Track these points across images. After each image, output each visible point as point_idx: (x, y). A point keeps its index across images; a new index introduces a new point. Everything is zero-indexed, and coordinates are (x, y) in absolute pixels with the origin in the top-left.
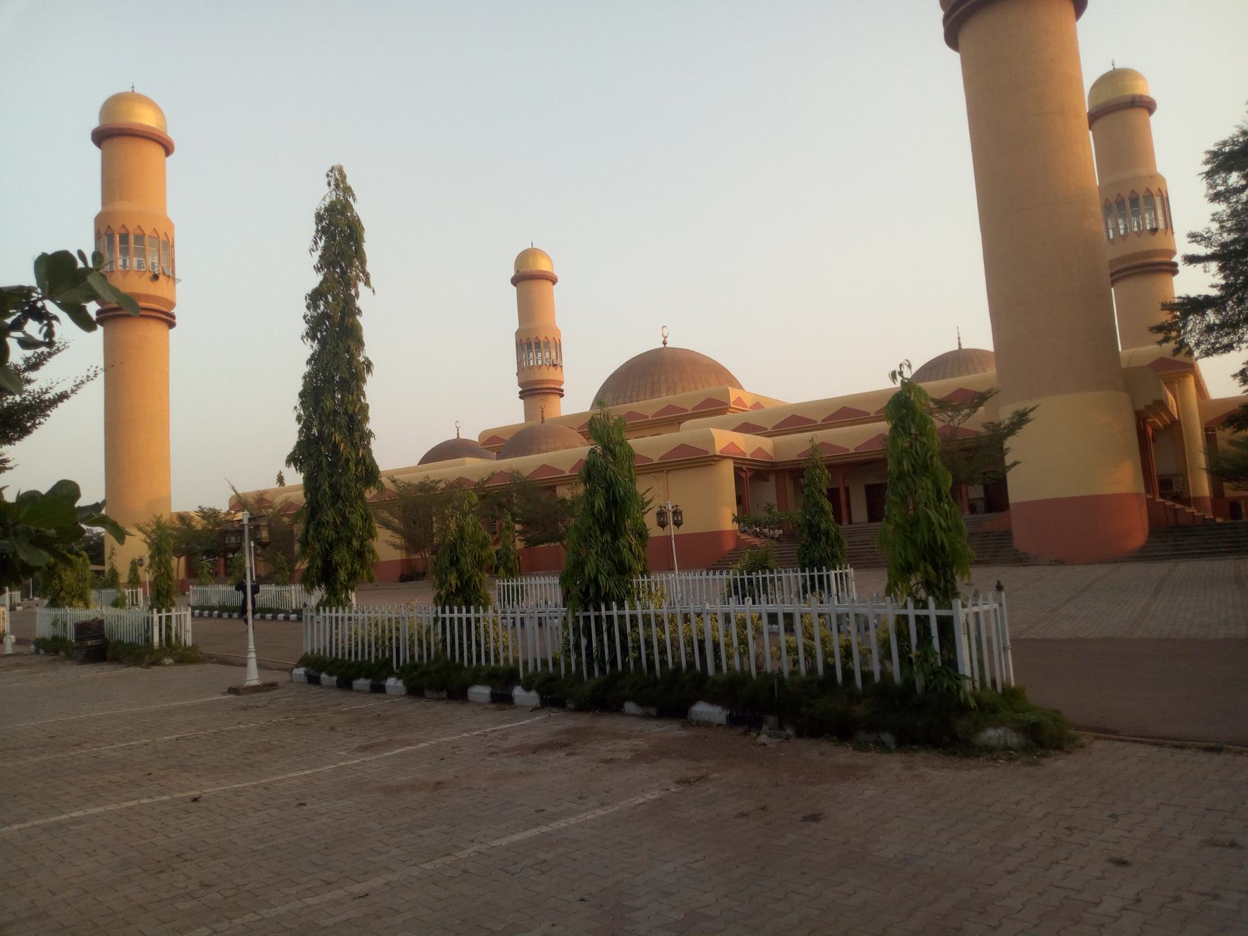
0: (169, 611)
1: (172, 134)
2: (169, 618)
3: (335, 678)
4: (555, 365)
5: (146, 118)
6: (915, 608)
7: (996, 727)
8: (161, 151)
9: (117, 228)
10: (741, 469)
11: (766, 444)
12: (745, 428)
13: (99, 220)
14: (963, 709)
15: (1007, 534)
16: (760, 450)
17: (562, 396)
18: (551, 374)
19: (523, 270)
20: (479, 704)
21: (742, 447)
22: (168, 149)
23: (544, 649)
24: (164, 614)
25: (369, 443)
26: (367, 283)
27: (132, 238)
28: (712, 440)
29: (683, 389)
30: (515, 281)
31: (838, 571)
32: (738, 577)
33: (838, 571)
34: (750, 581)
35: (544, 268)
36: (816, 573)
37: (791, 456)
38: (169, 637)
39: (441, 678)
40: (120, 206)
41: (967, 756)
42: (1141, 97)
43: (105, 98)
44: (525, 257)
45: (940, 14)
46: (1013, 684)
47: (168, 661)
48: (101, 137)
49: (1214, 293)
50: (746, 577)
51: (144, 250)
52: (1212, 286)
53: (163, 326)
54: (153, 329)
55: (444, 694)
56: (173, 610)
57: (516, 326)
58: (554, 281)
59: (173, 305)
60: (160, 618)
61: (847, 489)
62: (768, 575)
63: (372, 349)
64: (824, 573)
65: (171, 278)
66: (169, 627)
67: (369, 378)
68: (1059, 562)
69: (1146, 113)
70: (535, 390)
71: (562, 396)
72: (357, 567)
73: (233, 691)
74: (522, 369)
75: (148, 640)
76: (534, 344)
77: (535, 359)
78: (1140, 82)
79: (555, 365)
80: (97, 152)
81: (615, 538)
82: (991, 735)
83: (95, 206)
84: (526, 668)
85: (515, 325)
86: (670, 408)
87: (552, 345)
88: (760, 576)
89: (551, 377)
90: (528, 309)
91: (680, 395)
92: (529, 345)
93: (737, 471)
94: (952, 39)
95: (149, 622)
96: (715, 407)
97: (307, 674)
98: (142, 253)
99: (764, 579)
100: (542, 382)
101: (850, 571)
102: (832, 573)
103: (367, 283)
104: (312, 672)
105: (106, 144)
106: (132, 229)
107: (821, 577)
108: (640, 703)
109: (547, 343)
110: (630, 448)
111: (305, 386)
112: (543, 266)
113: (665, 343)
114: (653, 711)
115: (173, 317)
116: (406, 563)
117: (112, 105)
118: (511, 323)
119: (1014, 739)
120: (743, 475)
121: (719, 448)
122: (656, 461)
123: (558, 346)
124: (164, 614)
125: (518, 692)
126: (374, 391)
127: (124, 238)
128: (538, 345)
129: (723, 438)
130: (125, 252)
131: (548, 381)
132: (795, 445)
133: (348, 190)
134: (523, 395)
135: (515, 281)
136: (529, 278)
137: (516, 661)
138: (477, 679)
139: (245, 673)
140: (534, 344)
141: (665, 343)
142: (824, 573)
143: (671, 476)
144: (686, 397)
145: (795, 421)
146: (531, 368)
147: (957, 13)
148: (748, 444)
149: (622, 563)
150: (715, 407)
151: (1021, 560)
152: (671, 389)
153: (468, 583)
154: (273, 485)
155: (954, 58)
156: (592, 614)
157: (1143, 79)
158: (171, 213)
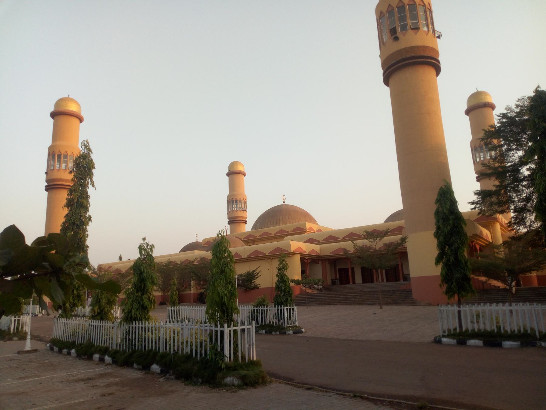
0: (20, 317)
1: (83, 114)
2: (19, 320)
4: (243, 210)
5: (73, 108)
7: (230, 377)
8: (78, 121)
9: (57, 152)
10: (305, 259)
11: (316, 248)
12: (310, 241)
13: (50, 148)
14: (221, 369)
15: (410, 291)
16: (313, 250)
17: (246, 223)
18: (242, 214)
21: (305, 249)
22: (81, 120)
24: (17, 318)
25: (87, 250)
26: (93, 186)
27: (62, 156)
28: (290, 246)
29: (290, 223)
31: (288, 307)
32: (255, 309)
33: (288, 307)
34: (257, 310)
35: (240, 170)
36: (279, 308)
37: (327, 253)
38: (18, 328)
39: (86, 350)
40: (58, 143)
41: (214, 387)
42: (488, 103)
43: (56, 101)
44: (233, 165)
45: (382, 71)
46: (255, 359)
47: (15, 338)
48: (54, 115)
49: (494, 189)
50: (255, 309)
51: (67, 161)
52: (494, 186)
55: (86, 357)
56: (21, 316)
57: (228, 193)
58: (245, 175)
59: (246, 218)
60: (15, 320)
61: (402, 264)
62: (266, 308)
63: (92, 211)
64: (282, 308)
66: (18, 324)
67: (90, 223)
68: (429, 305)
69: (491, 109)
70: (234, 221)
71: (246, 223)
72: (76, 302)
73: (19, 353)
74: (229, 212)
75: (9, 329)
76: (235, 201)
78: (488, 97)
79: (243, 210)
80: (52, 121)
81: (143, 294)
82: (228, 380)
83: (49, 142)
85: (227, 193)
86: (282, 231)
87: (242, 202)
88: (260, 308)
89: (242, 215)
90: (232, 186)
91: (288, 225)
93: (302, 260)
94: (386, 81)
95: (11, 321)
96: (299, 231)
97: (50, 346)
99: (262, 310)
100: (238, 217)
101: (295, 307)
102: (285, 308)
103: (93, 186)
104: (52, 346)
105: (56, 118)
106: (63, 152)
107: (281, 309)
108: (138, 364)
109: (240, 201)
110: (230, 252)
112: (240, 168)
113: (284, 202)
114: (141, 367)
116: (163, 297)
118: (226, 192)
119: (236, 382)
120: (306, 261)
121: (293, 250)
122: (267, 254)
123: (245, 202)
124: (17, 318)
125: (106, 357)
126: (91, 229)
127: (59, 156)
128: (236, 202)
129: (296, 244)
130: (59, 161)
131: (240, 217)
132: (330, 249)
133: (89, 150)
135: (467, 112)
136: (234, 173)
138: (95, 352)
139: (25, 344)
140: (235, 201)
141: (284, 202)
142: (282, 308)
144: (288, 226)
145: (331, 238)
146: (233, 211)
147: (388, 71)
148: (307, 248)
149: (143, 305)
150: (299, 231)
151: (413, 303)
152: (284, 223)
153: (102, 311)
154: (117, 260)
155: (387, 89)
156: (131, 326)
157: (489, 95)
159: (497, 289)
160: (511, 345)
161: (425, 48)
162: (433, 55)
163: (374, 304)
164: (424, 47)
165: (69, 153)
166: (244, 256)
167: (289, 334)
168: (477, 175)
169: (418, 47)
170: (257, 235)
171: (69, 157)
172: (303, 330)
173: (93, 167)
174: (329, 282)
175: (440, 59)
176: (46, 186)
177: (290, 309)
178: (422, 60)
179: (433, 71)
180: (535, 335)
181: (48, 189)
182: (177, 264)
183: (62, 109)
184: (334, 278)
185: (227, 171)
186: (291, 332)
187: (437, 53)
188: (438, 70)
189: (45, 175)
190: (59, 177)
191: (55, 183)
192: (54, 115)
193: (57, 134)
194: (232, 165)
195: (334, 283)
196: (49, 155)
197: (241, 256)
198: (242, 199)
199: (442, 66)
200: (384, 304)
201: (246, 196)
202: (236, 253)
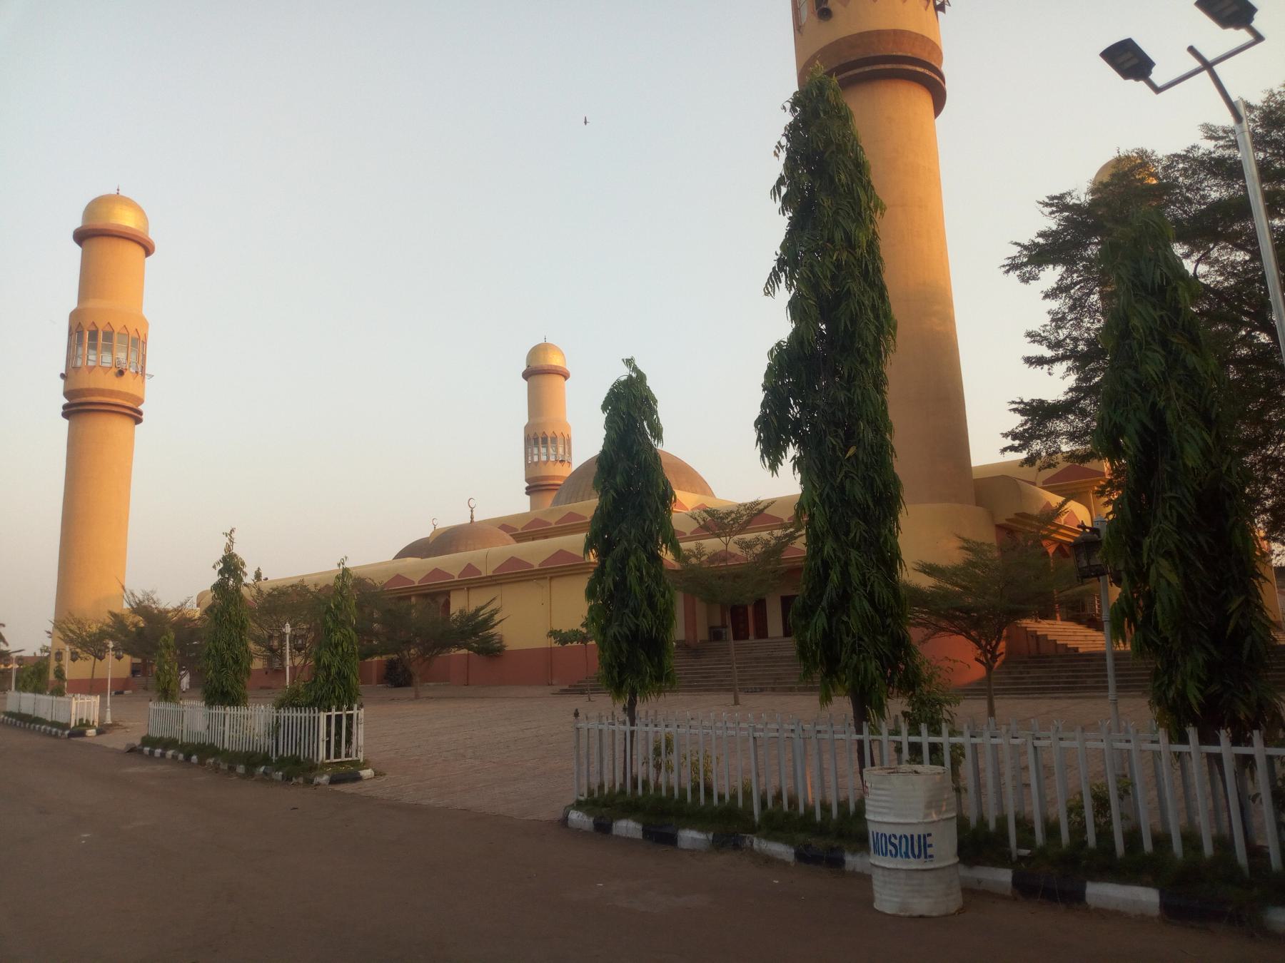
1: (153, 235)
3: (711, 836)
5: (126, 219)
6: (1266, 744)
8: (140, 251)
18: (126, 385)
19: (534, 365)
20: (1003, 897)
22: (148, 250)
23: (1000, 805)
27: (101, 335)
30: (526, 375)
35: (554, 363)
40: (91, 304)
44: (537, 352)
48: (81, 237)
51: (112, 346)
53: (128, 423)
54: (118, 425)
57: (526, 421)
58: (566, 376)
59: (141, 401)
65: (141, 372)
74: (528, 466)
77: (542, 454)
80: (77, 250)
84: (764, 804)
90: (536, 404)
92: (536, 440)
98: (110, 349)
100: (547, 478)
105: (87, 242)
106: (101, 326)
109: (554, 440)
111: (609, 424)
112: (555, 361)
115: (141, 413)
117: (95, 207)
118: (520, 417)
122: (536, 567)
123: (138, 343)
127: (94, 335)
128: (545, 441)
134: (529, 491)
135: (526, 375)
137: (1002, 822)
142: (355, 712)
143: (554, 582)
158: (148, 311)
159: (1071, 656)
160: (694, 840)
161: (898, 35)
162: (924, 56)
163: (762, 690)
164: (895, 32)
165: (117, 328)
166: (487, 571)
167: (319, 784)
168: (66, 401)
169: (879, 33)
170: (553, 520)
171: (116, 336)
172: (366, 773)
173: (1041, 402)
174: (702, 634)
175: (945, 69)
176: (65, 407)
177: (339, 718)
178: (888, 66)
179: (923, 100)
180: (752, 813)
181: (68, 412)
182: (308, 591)
183: (99, 223)
184: (718, 622)
185: (524, 368)
186: (325, 778)
187: (936, 49)
188: (939, 100)
189: (62, 382)
190: (92, 386)
191: (84, 399)
192: (81, 237)
193: (89, 283)
194: (536, 352)
195: (716, 635)
196: (70, 334)
197: (480, 573)
198: (558, 434)
199: (949, 86)
200: (741, 690)
201: (568, 427)
202: (469, 564)
